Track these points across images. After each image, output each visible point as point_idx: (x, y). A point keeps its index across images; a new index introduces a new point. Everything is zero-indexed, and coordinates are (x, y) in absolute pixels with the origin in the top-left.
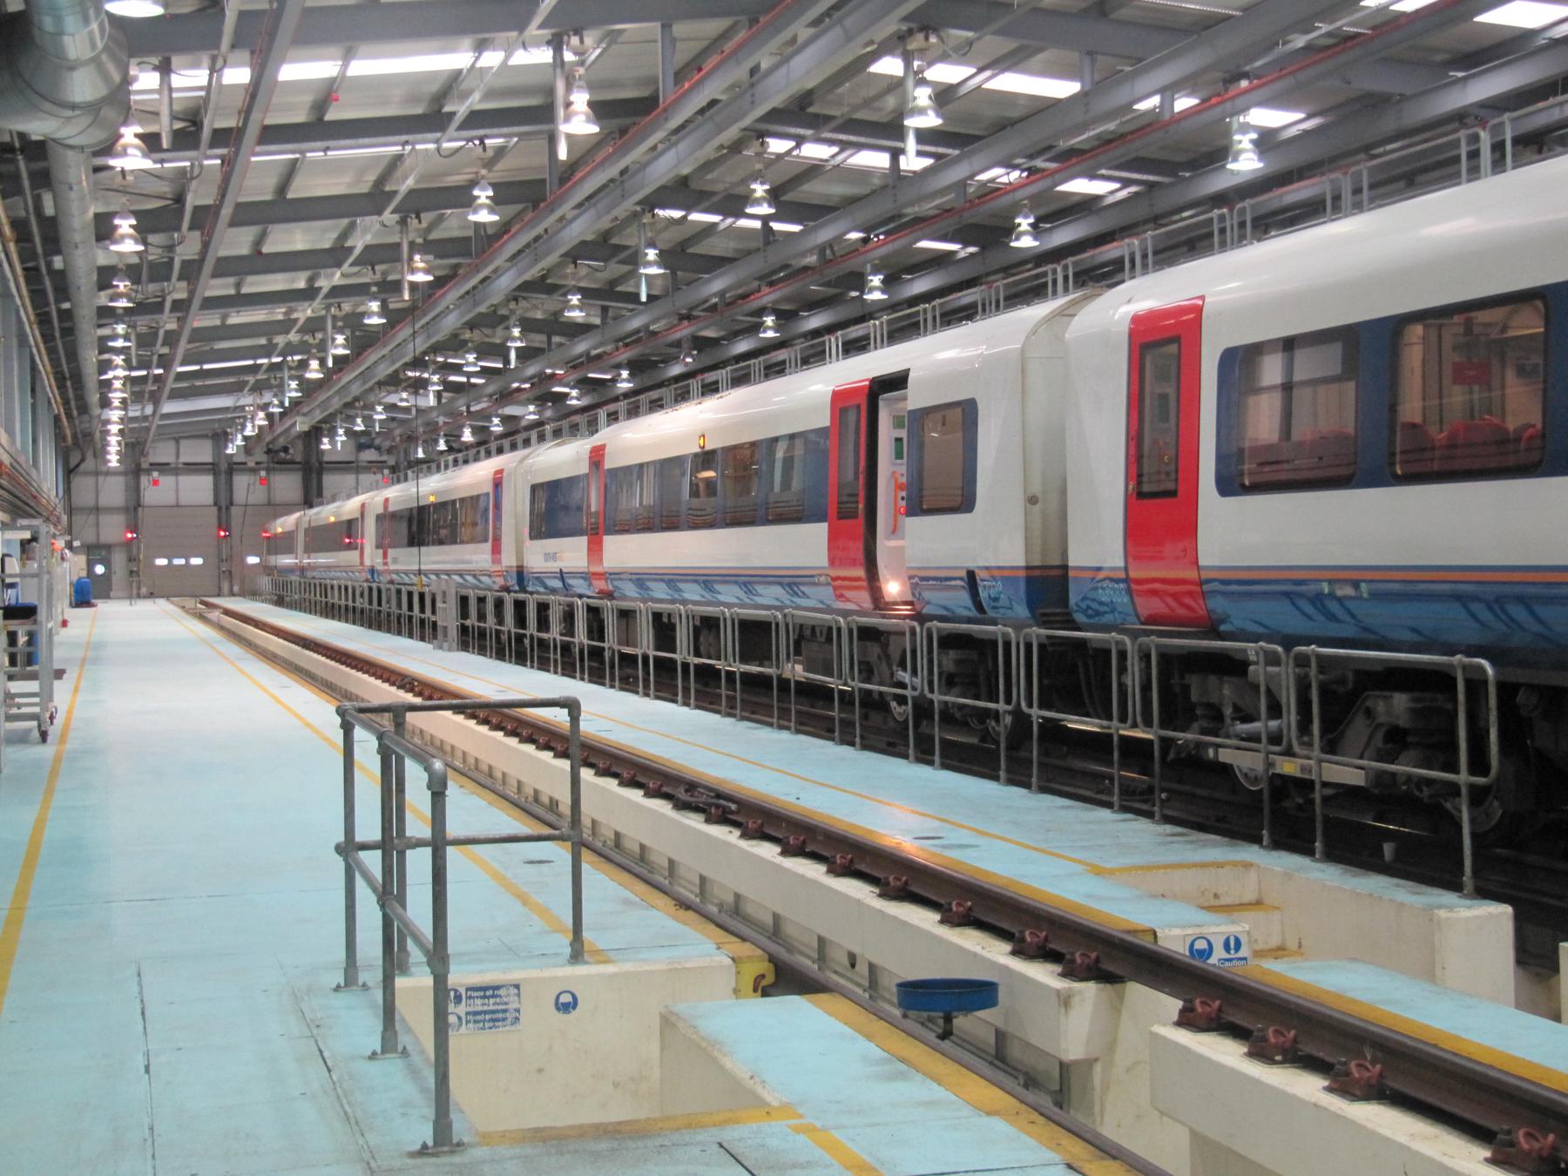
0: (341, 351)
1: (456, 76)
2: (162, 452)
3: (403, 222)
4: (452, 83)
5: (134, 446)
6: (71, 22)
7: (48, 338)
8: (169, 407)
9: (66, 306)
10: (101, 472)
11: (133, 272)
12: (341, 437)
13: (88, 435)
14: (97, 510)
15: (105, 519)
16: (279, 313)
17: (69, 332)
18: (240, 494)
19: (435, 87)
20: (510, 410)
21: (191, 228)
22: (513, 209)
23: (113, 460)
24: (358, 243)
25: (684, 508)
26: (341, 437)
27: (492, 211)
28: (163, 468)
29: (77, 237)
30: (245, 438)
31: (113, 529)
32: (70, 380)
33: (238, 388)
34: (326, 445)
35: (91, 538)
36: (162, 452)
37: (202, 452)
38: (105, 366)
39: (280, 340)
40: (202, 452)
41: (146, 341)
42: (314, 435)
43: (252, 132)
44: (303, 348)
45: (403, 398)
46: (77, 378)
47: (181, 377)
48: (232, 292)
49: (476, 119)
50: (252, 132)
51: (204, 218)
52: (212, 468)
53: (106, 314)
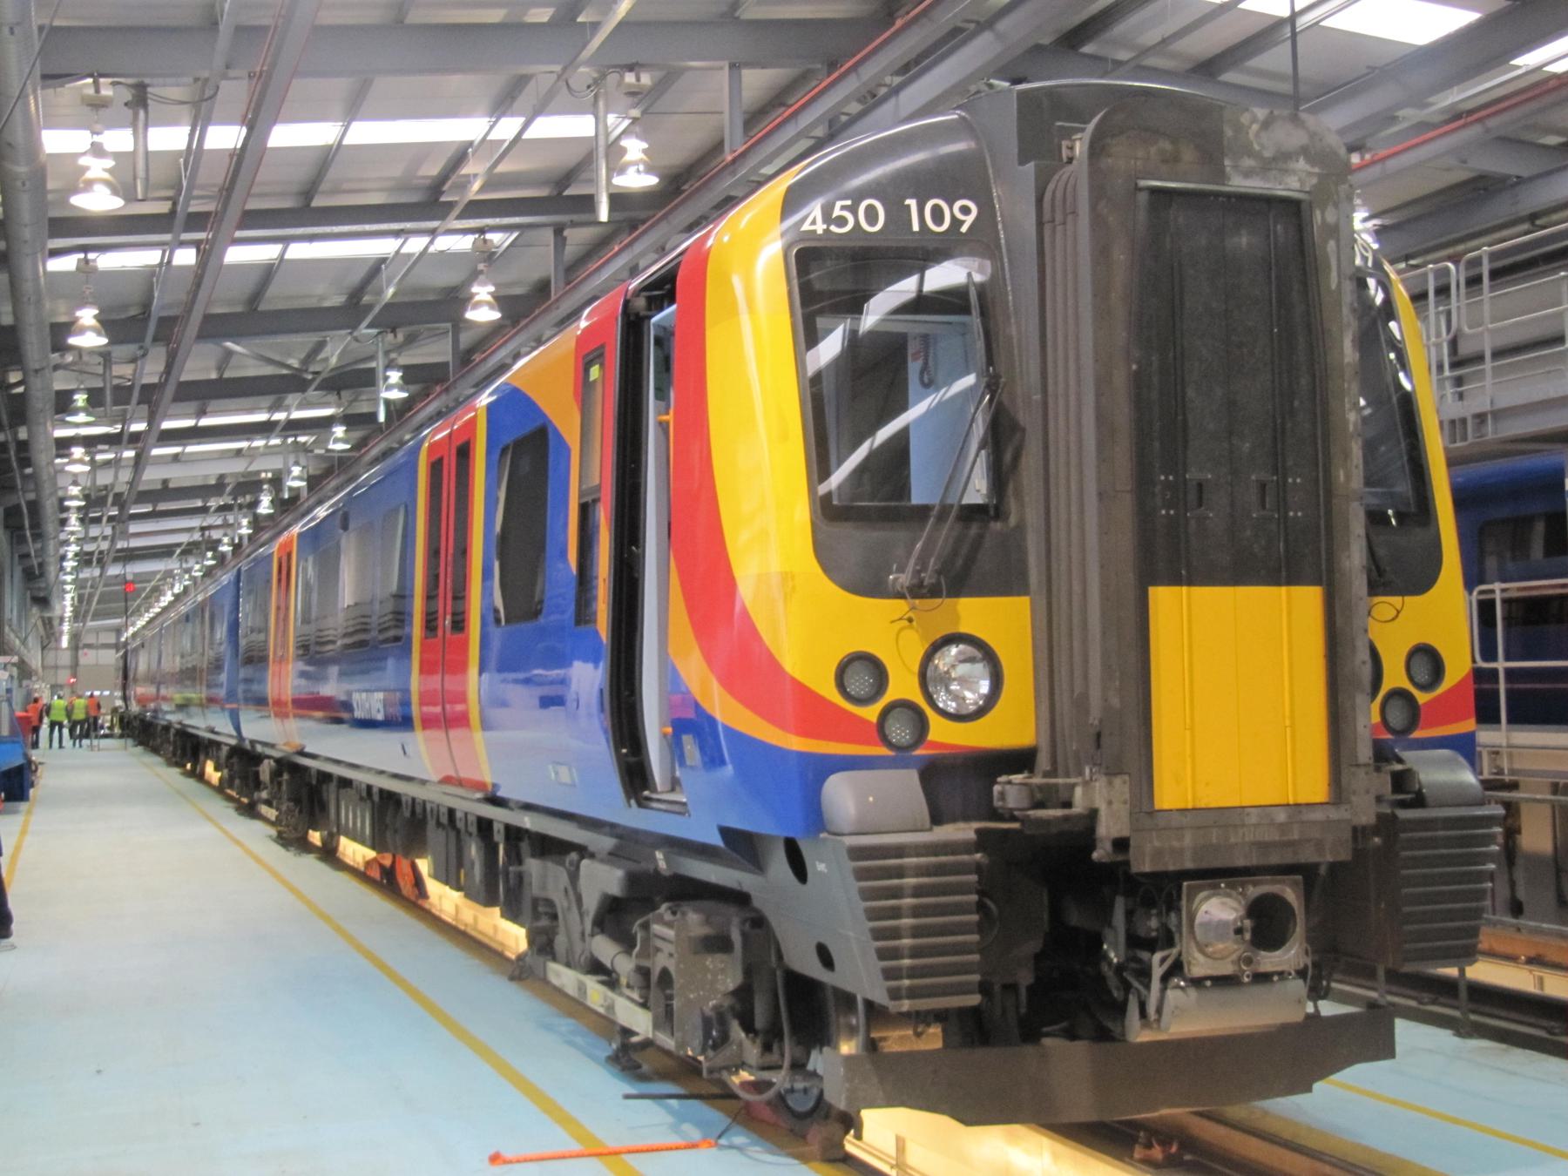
0: (397, 395)
5: (75, 637)
9: (29, 471)
10: (58, 648)
14: (56, 667)
19: (356, 278)
21: (155, 340)
22: (414, 388)
27: (401, 389)
28: (89, 646)
29: (39, 405)
31: (64, 676)
39: (213, 503)
40: (112, 639)
43: (234, 213)
48: (214, 376)
50: (234, 213)
51: (168, 330)
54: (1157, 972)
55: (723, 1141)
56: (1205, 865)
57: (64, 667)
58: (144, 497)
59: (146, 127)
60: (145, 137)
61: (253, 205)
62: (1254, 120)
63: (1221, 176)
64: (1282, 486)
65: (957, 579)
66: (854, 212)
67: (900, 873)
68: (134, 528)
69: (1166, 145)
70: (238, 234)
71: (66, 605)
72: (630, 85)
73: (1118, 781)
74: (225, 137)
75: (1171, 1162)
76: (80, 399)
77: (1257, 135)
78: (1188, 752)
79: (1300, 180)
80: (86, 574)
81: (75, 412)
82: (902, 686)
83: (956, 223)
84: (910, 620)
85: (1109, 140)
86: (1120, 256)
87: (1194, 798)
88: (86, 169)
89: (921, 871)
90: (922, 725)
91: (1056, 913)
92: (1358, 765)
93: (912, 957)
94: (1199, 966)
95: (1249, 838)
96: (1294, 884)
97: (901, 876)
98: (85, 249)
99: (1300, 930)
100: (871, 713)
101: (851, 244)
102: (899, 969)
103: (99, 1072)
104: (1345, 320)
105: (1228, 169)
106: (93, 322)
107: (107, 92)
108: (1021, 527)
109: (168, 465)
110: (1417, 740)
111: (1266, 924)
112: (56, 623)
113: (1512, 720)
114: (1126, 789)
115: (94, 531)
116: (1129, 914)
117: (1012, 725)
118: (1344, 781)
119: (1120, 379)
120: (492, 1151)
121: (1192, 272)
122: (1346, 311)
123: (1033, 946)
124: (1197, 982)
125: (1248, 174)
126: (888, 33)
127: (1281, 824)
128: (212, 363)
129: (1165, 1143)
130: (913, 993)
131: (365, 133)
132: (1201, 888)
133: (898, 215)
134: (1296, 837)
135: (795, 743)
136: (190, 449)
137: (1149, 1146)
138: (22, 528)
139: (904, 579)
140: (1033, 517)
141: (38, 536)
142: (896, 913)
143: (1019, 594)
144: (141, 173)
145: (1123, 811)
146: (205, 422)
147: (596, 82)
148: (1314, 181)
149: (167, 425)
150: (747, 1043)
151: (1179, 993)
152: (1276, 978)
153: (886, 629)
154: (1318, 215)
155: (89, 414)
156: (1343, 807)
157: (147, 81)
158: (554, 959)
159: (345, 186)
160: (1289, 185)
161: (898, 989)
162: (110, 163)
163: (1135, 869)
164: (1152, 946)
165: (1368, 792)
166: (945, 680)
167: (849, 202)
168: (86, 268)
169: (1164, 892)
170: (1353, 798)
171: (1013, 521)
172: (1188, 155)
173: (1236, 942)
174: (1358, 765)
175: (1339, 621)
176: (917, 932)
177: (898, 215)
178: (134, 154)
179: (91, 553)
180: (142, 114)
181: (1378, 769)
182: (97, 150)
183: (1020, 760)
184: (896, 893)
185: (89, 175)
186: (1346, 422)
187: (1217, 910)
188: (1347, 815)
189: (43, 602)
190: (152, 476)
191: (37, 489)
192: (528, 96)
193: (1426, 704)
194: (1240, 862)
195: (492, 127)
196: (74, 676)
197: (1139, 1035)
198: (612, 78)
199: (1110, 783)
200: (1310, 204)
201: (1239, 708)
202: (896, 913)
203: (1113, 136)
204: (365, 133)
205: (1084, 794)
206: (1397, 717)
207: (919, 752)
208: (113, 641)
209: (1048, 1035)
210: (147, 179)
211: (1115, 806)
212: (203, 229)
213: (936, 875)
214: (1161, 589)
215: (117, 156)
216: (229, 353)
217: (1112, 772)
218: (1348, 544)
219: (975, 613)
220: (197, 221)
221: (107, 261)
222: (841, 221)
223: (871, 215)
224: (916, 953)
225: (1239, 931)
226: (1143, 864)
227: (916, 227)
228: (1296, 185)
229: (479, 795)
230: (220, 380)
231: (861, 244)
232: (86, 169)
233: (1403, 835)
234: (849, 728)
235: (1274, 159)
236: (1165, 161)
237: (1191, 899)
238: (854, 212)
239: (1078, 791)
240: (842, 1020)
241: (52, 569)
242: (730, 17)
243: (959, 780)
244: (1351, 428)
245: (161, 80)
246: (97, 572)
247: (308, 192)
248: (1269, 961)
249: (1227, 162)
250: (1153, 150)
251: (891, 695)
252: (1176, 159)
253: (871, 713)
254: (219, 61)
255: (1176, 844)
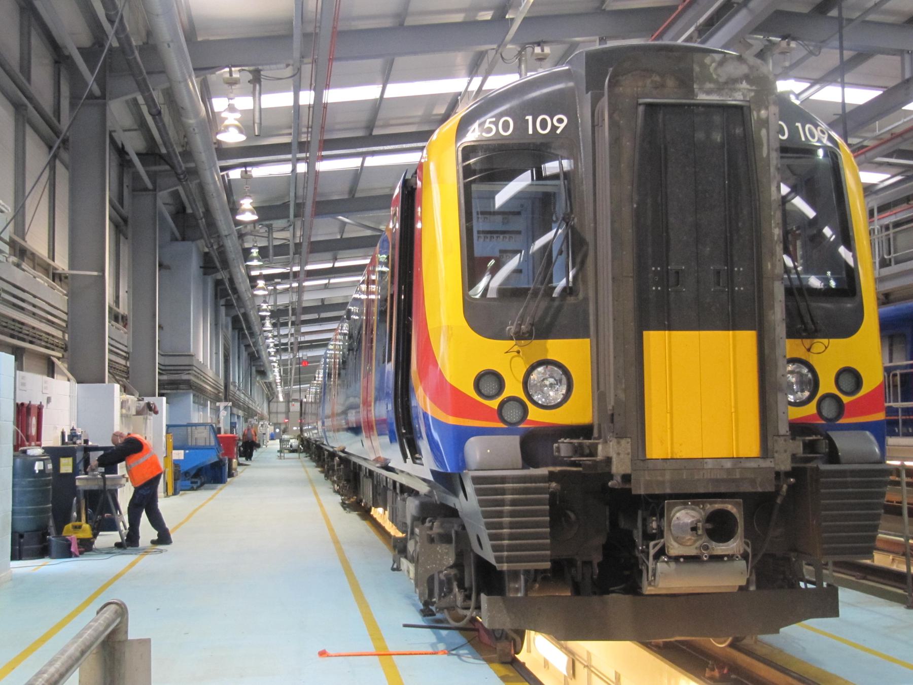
10: (278, 402)
14: (277, 413)
15: (279, 416)
23: (281, 399)
25: (39, 546)
31: (281, 418)
35: (275, 421)
48: (339, 237)
54: (652, 552)
55: (454, 652)
56: (676, 491)
57: (281, 413)
58: (307, 310)
59: (260, 94)
60: (260, 100)
62: (713, 61)
63: (691, 93)
64: (731, 274)
65: (543, 329)
66: (497, 125)
67: (503, 492)
68: (304, 329)
69: (657, 78)
70: (324, 153)
71: (276, 375)
72: (538, 54)
73: (623, 442)
74: (307, 97)
75: (724, 678)
76: (255, 252)
77: (716, 69)
78: (669, 426)
79: (743, 94)
80: (285, 357)
81: (252, 259)
82: (513, 389)
83: (554, 128)
84: (518, 352)
85: (620, 78)
86: (627, 142)
87: (672, 453)
88: (226, 119)
89: (514, 491)
90: (525, 411)
91: (614, 524)
92: (779, 436)
93: (509, 540)
94: (675, 549)
95: (707, 476)
96: (736, 505)
97: (504, 494)
98: (245, 165)
99: (740, 530)
100: (494, 404)
101: (512, 142)
102: (502, 546)
104: (772, 175)
105: (696, 90)
106: (250, 207)
107: (236, 75)
108: (586, 299)
109: (314, 291)
110: (840, 424)
111: (719, 527)
112: (274, 386)
114: (629, 446)
115: (284, 331)
116: (644, 520)
117: (579, 410)
118: (770, 444)
119: (627, 212)
120: (321, 649)
121: (672, 150)
122: (772, 170)
123: (600, 540)
124: (676, 559)
125: (708, 92)
126: (674, 15)
127: (728, 469)
128: (336, 229)
129: (721, 668)
130: (510, 560)
131: (395, 90)
132: (675, 505)
133: (521, 125)
134: (738, 476)
135: (452, 420)
136: (332, 281)
137: (713, 670)
138: (242, 329)
139: (511, 329)
140: (591, 294)
141: (252, 334)
142: (500, 514)
143: (583, 337)
144: (257, 120)
145: (627, 459)
146: (338, 264)
147: (520, 53)
148: (753, 94)
149: (309, 267)
150: (458, 594)
151: (665, 565)
152: (726, 559)
153: (504, 357)
154: (755, 114)
155: (259, 261)
156: (768, 461)
157: (260, 67)
158: (406, 557)
159: (392, 122)
160: (736, 98)
161: (502, 557)
162: (238, 115)
163: (634, 492)
164: (653, 537)
165: (785, 451)
166: (540, 387)
167: (494, 119)
168: (246, 176)
169: (656, 505)
170: (776, 455)
171: (581, 296)
172: (671, 82)
173: (692, 535)
174: (779, 436)
175: (767, 351)
176: (512, 526)
177: (521, 125)
178: (254, 110)
179: (286, 344)
180: (258, 87)
181: (793, 439)
182: (231, 109)
183: (584, 431)
184: (501, 503)
185: (226, 123)
186: (772, 235)
187: (684, 516)
188: (772, 465)
189: (263, 373)
190: (309, 299)
191: (244, 306)
192: (484, 66)
193: (848, 403)
194: (701, 490)
195: (469, 83)
196: (288, 418)
197: (648, 590)
198: (529, 50)
199: (618, 443)
200: (749, 107)
201: (702, 399)
202: (500, 514)
203: (622, 76)
204: (395, 90)
205: (603, 449)
206: (829, 410)
207: (521, 426)
209: (613, 592)
210: (260, 123)
211: (622, 456)
212: (289, 153)
213: (523, 494)
214: (652, 333)
215: (243, 112)
216: (344, 224)
217: (620, 436)
218: (773, 305)
219: (556, 348)
220: (303, 146)
221: (257, 172)
222: (489, 130)
223: (506, 126)
224: (512, 537)
225: (694, 529)
226: (639, 489)
227: (530, 132)
228: (741, 98)
229: (378, 465)
230: (342, 240)
231: (500, 142)
232: (226, 119)
233: (822, 480)
234: (484, 413)
235: (726, 83)
236: (656, 88)
237: (670, 510)
238: (497, 125)
239: (600, 447)
240: (512, 585)
241: (264, 354)
242: (600, 11)
243: (535, 444)
244: (776, 238)
245: (268, 67)
246: (292, 356)
247: (370, 126)
248: (720, 549)
249: (695, 86)
250: (648, 81)
251: (506, 394)
252: (663, 86)
253: (494, 404)
254: (296, 54)
255: (660, 478)
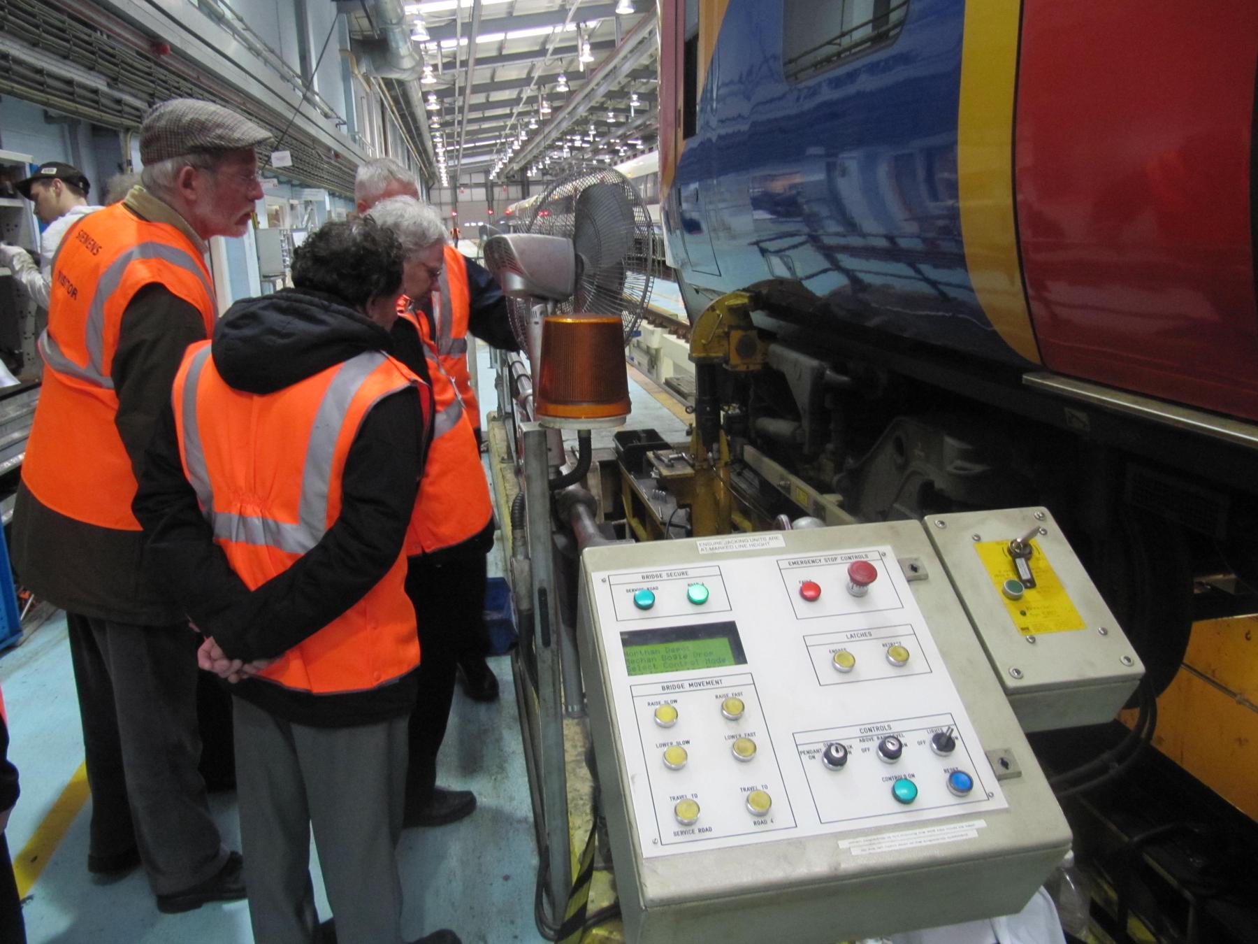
1: (548, 36)
2: (465, 179)
3: (539, 88)
4: (547, 39)
5: (453, 178)
6: (401, 44)
7: (412, 138)
8: (464, 161)
11: (439, 113)
12: (535, 170)
13: (434, 173)
16: (507, 111)
17: (420, 135)
18: (496, 196)
19: (541, 40)
20: (601, 157)
23: (445, 183)
24: (524, 96)
26: (535, 170)
28: (465, 186)
30: (514, 151)
32: (423, 152)
33: (490, 152)
34: (529, 174)
36: (465, 179)
37: (480, 179)
38: (433, 137)
40: (480, 179)
41: (450, 136)
42: (524, 169)
44: (511, 135)
45: (556, 155)
46: (425, 151)
47: (465, 149)
49: (557, 51)
52: (485, 185)
53: (430, 114)
61: (479, 56)
103: (516, 937)
113: (23, 163)
208: (482, 181)
247: (510, 14)
